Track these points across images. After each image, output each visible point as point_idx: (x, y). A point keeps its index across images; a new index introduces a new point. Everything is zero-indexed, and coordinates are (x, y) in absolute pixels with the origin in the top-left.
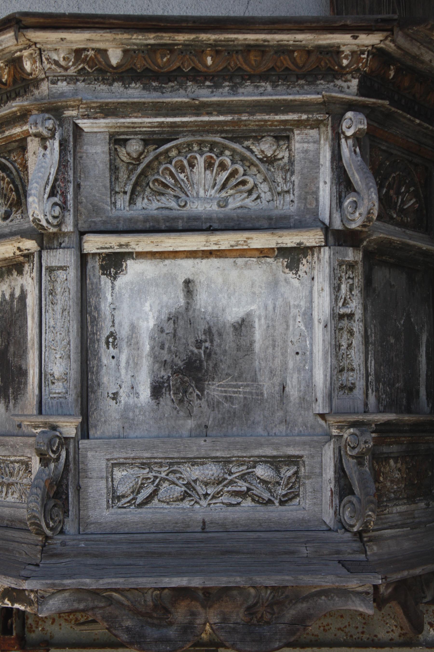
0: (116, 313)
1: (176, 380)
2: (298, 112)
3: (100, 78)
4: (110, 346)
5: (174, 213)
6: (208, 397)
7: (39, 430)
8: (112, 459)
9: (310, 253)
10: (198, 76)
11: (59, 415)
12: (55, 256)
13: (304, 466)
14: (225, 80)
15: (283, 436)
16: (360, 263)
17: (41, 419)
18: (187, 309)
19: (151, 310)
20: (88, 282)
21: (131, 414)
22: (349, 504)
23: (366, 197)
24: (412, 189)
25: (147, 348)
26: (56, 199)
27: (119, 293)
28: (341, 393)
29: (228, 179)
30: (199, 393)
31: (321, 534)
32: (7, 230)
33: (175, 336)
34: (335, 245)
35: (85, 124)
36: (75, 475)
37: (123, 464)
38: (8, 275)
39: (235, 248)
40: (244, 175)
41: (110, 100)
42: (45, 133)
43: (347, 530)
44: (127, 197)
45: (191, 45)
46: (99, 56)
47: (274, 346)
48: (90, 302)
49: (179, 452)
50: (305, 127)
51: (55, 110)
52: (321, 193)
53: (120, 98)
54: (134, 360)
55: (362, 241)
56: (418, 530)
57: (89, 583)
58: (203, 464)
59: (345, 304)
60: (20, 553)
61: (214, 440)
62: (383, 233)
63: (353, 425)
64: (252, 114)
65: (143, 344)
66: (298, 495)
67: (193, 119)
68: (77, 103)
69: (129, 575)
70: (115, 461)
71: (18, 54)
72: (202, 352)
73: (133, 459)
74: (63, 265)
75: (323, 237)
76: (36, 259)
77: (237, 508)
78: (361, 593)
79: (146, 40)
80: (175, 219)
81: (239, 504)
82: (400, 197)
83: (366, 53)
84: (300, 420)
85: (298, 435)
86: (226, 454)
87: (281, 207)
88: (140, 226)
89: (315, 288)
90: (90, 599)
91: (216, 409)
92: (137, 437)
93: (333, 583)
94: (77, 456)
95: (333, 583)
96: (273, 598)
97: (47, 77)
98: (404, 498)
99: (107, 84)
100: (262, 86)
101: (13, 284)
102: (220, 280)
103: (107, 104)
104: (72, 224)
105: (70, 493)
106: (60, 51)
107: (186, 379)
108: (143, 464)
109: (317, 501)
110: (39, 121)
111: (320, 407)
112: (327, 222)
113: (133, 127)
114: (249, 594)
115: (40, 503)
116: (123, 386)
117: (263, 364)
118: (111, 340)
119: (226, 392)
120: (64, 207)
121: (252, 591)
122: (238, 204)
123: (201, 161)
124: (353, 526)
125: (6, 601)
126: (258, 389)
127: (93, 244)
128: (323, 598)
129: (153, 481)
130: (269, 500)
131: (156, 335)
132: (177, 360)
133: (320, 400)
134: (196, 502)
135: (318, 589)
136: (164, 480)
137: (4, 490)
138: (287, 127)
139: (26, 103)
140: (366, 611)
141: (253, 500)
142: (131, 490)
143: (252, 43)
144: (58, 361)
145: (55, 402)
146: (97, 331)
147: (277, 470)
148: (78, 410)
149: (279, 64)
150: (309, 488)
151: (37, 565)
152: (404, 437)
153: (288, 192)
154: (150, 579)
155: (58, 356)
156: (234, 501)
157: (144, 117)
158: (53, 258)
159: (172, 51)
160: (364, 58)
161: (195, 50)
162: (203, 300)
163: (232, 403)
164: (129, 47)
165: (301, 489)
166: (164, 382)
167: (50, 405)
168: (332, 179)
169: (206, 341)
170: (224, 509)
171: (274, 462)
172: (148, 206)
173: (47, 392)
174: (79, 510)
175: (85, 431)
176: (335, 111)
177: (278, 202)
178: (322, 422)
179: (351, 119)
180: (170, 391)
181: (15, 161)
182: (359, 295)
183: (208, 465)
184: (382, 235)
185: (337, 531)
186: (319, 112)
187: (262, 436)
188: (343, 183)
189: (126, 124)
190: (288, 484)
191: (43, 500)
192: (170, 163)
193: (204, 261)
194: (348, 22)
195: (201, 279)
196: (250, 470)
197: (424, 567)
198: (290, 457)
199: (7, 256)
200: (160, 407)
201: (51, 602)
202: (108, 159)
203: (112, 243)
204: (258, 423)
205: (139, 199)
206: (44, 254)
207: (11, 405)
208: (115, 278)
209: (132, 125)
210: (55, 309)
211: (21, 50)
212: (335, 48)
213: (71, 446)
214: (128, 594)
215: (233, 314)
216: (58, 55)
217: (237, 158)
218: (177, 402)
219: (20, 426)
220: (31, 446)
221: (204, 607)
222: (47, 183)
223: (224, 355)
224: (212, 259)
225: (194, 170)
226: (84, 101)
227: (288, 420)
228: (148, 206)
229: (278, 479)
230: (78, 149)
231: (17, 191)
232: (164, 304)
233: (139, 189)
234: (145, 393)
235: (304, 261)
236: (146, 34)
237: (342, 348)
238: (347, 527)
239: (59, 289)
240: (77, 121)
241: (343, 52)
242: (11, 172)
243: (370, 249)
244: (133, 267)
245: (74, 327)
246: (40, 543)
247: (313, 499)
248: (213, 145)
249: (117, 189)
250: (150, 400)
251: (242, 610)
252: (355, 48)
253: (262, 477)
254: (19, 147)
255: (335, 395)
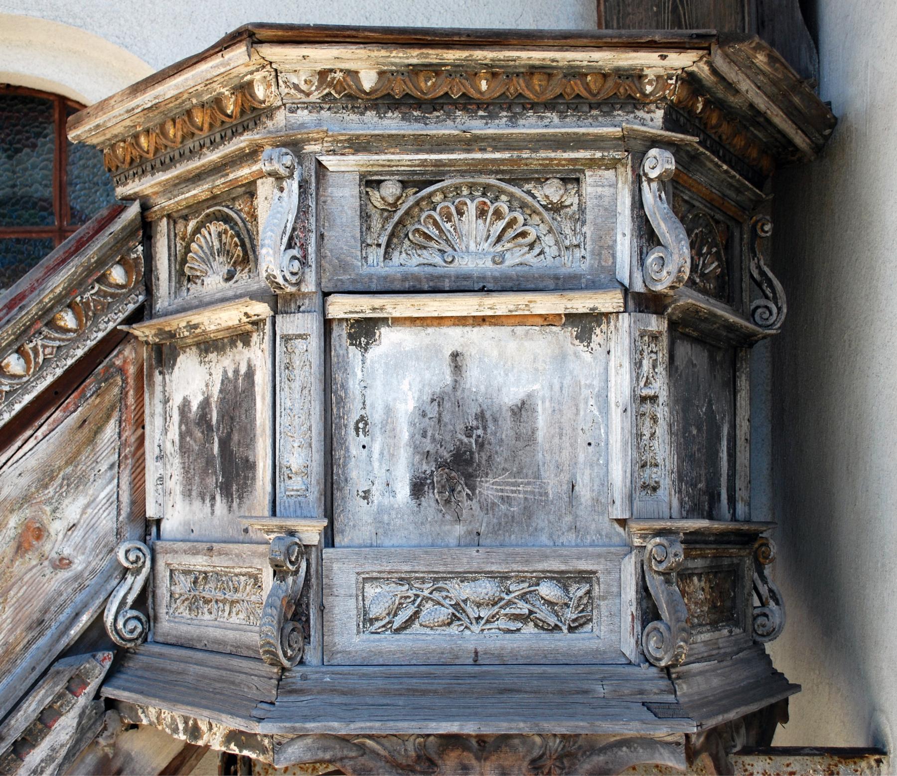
0: (368, 392)
1: (442, 475)
2: (591, 149)
3: (350, 106)
4: (361, 433)
5: (439, 271)
6: (481, 497)
7: (273, 536)
8: (363, 573)
9: (605, 320)
10: (468, 104)
11: (297, 517)
12: (293, 322)
13: (599, 584)
14: (502, 109)
15: (573, 547)
16: (665, 334)
17: (276, 522)
18: (455, 388)
19: (410, 389)
20: (333, 353)
21: (386, 518)
22: (655, 632)
23: (676, 251)
24: (714, 250)
25: (405, 435)
26: (295, 252)
27: (372, 368)
28: (643, 493)
29: (504, 230)
30: (470, 492)
31: (620, 669)
32: (231, 293)
33: (439, 421)
34: (635, 311)
35: (330, 162)
36: (317, 593)
37: (376, 579)
38: (231, 348)
39: (514, 313)
40: (524, 225)
41: (361, 132)
42: (283, 171)
43: (651, 665)
44: (382, 250)
45: (462, 66)
46: (348, 79)
47: (561, 435)
48: (335, 379)
49: (445, 565)
50: (599, 168)
51: (293, 145)
52: (619, 247)
53: (374, 130)
54: (389, 451)
55: (666, 307)
56: (725, 663)
57: (339, 728)
58: (475, 580)
59: (647, 384)
60: (249, 688)
61: (488, 550)
62: (692, 298)
63: (660, 533)
64: (534, 150)
65: (401, 431)
66: (591, 620)
67: (463, 156)
68: (321, 135)
69: (386, 718)
70: (367, 576)
71: (249, 77)
72: (473, 441)
73: (389, 572)
74: (302, 333)
75: (622, 301)
76: (268, 328)
77: (516, 635)
78: (671, 743)
79: (407, 58)
80: (441, 277)
81: (519, 630)
82: (702, 259)
83: (674, 78)
84: (593, 526)
85: (591, 546)
86: (503, 568)
87: (570, 264)
88: (397, 286)
89: (612, 364)
90: (337, 746)
91: (490, 512)
92: (393, 546)
93: (637, 730)
94: (320, 568)
95: (637, 730)
96: (562, 749)
97: (284, 105)
98: (707, 624)
99: (357, 113)
100: (547, 118)
101: (237, 358)
102: (495, 353)
103: (358, 137)
104: (314, 283)
105: (311, 615)
106: (301, 73)
107: (453, 474)
108: (401, 579)
109: (615, 628)
110: (275, 156)
111: (619, 512)
112: (626, 283)
113: (389, 166)
114: (534, 743)
115: (276, 626)
116: (376, 482)
117: (548, 458)
118: (361, 425)
119: (502, 490)
120: (304, 261)
121: (538, 740)
122: (518, 261)
123: (471, 208)
124: (659, 660)
125: (232, 746)
126: (541, 488)
127: (340, 307)
128: (624, 749)
129: (415, 600)
130: (556, 625)
131: (416, 420)
132: (441, 450)
133: (618, 502)
134: (466, 627)
135: (618, 738)
136: (427, 599)
137: (227, 608)
138: (577, 167)
139: (257, 137)
140: (677, 766)
141: (536, 625)
142: (387, 612)
143: (537, 63)
144: (297, 450)
145: (292, 501)
146: (344, 414)
147: (566, 589)
148: (321, 511)
149: (568, 90)
150: (604, 611)
151: (272, 704)
152: (710, 549)
153: (578, 246)
154: (413, 723)
155: (296, 445)
156: (513, 626)
157: (402, 154)
158: (288, 325)
159: (437, 74)
160: (671, 84)
161: (466, 72)
162: (473, 377)
163: (510, 505)
164: (386, 68)
165: (595, 612)
166: (426, 479)
167: (287, 504)
168: (632, 230)
169: (478, 428)
170: (500, 637)
171: (562, 579)
172: (408, 261)
173: (283, 489)
174: (323, 635)
175: (329, 537)
176: (637, 148)
177: (566, 258)
178: (620, 530)
179: (655, 158)
180: (434, 489)
181: (241, 210)
182: (664, 373)
183: (481, 581)
184: (690, 301)
185: (639, 665)
186: (616, 148)
187: (546, 546)
188: (647, 235)
189: (381, 162)
190: (579, 606)
191: (279, 623)
192: (434, 209)
193: (476, 329)
194: (657, 38)
195: (471, 354)
196: (532, 589)
197: (738, 710)
198: (580, 572)
199: (230, 324)
200: (422, 509)
201: (290, 750)
202: (358, 204)
203: (364, 306)
204: (542, 529)
205: (396, 254)
206: (279, 318)
207: (235, 505)
208: (366, 350)
209: (388, 163)
210: (293, 386)
211: (252, 73)
212: (637, 72)
213: (313, 556)
214: (384, 741)
215: (511, 396)
216: (298, 77)
217: (516, 204)
218: (443, 502)
219: (246, 531)
220: (262, 555)
221: (478, 759)
222: (284, 232)
223: (500, 446)
224: (485, 327)
225: (463, 219)
226: (330, 133)
227: (578, 527)
228: (408, 261)
229: (567, 600)
230: (321, 193)
231: (243, 245)
232: (427, 382)
233: (395, 240)
234: (403, 491)
235: (598, 331)
236: (408, 51)
237: (644, 437)
238: (652, 661)
239: (298, 362)
240: (320, 158)
241: (646, 76)
242: (236, 224)
243: (674, 318)
244: (387, 336)
245: (317, 409)
246: (275, 676)
247: (609, 625)
248: (486, 188)
249: (369, 241)
250: (410, 501)
251: (525, 764)
252: (662, 72)
253: (547, 598)
254: (246, 193)
255: (636, 495)
